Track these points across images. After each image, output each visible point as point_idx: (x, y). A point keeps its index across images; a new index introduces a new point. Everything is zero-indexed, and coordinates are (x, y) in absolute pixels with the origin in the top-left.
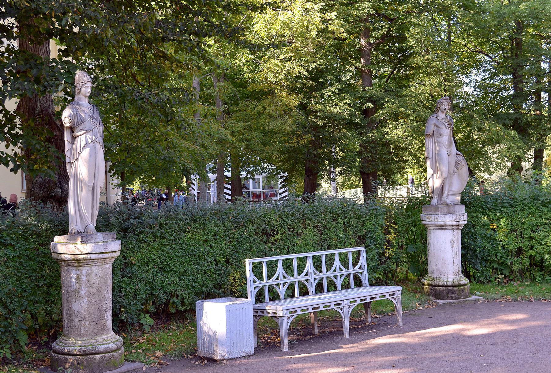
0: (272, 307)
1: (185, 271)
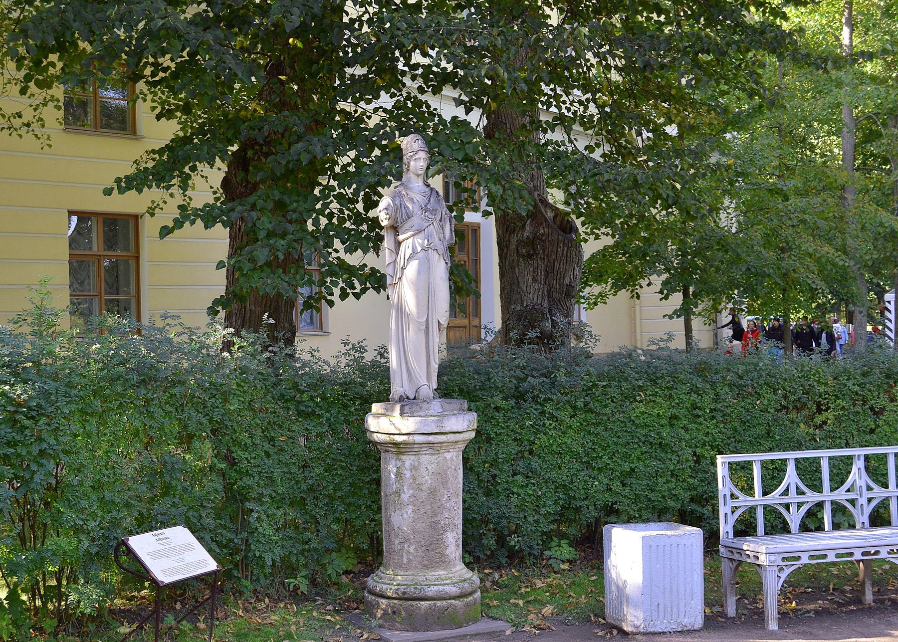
0: (752, 545)
1: (633, 470)
